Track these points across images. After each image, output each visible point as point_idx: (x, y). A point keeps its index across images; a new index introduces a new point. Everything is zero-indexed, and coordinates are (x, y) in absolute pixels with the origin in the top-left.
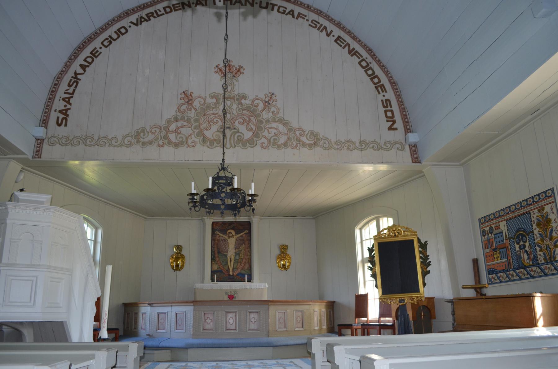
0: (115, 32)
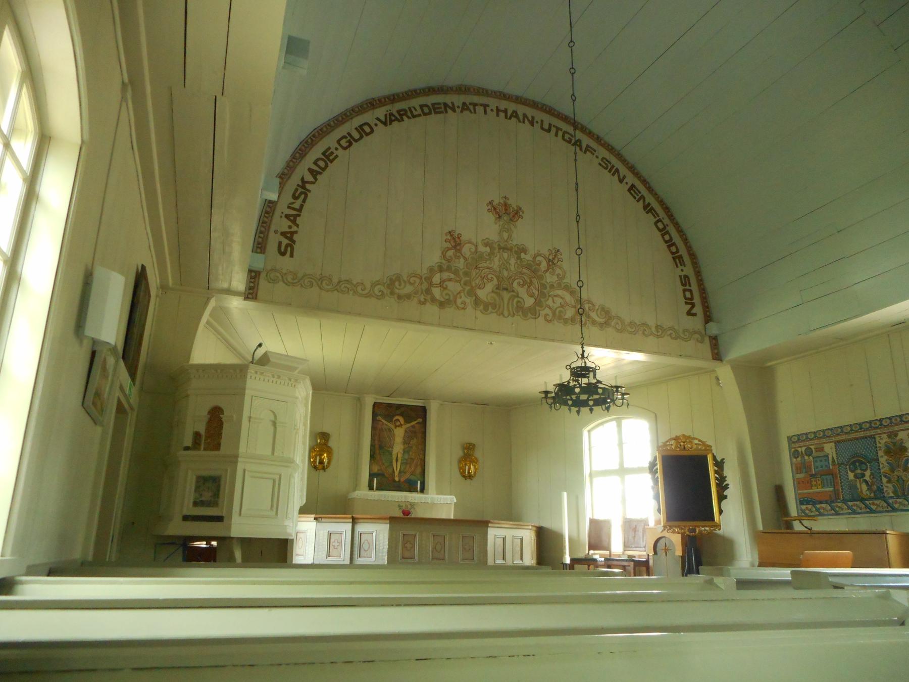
0: (356, 129)
